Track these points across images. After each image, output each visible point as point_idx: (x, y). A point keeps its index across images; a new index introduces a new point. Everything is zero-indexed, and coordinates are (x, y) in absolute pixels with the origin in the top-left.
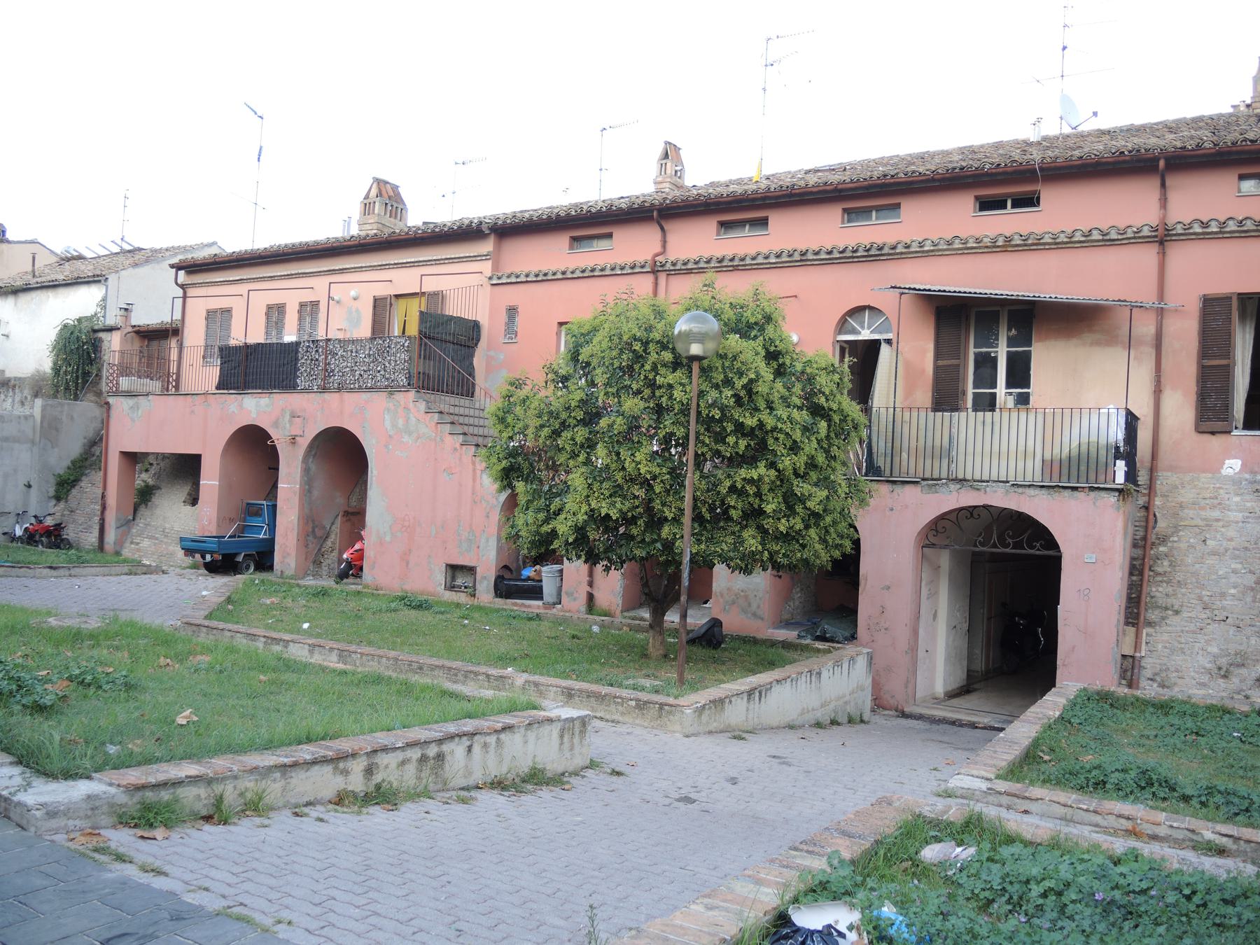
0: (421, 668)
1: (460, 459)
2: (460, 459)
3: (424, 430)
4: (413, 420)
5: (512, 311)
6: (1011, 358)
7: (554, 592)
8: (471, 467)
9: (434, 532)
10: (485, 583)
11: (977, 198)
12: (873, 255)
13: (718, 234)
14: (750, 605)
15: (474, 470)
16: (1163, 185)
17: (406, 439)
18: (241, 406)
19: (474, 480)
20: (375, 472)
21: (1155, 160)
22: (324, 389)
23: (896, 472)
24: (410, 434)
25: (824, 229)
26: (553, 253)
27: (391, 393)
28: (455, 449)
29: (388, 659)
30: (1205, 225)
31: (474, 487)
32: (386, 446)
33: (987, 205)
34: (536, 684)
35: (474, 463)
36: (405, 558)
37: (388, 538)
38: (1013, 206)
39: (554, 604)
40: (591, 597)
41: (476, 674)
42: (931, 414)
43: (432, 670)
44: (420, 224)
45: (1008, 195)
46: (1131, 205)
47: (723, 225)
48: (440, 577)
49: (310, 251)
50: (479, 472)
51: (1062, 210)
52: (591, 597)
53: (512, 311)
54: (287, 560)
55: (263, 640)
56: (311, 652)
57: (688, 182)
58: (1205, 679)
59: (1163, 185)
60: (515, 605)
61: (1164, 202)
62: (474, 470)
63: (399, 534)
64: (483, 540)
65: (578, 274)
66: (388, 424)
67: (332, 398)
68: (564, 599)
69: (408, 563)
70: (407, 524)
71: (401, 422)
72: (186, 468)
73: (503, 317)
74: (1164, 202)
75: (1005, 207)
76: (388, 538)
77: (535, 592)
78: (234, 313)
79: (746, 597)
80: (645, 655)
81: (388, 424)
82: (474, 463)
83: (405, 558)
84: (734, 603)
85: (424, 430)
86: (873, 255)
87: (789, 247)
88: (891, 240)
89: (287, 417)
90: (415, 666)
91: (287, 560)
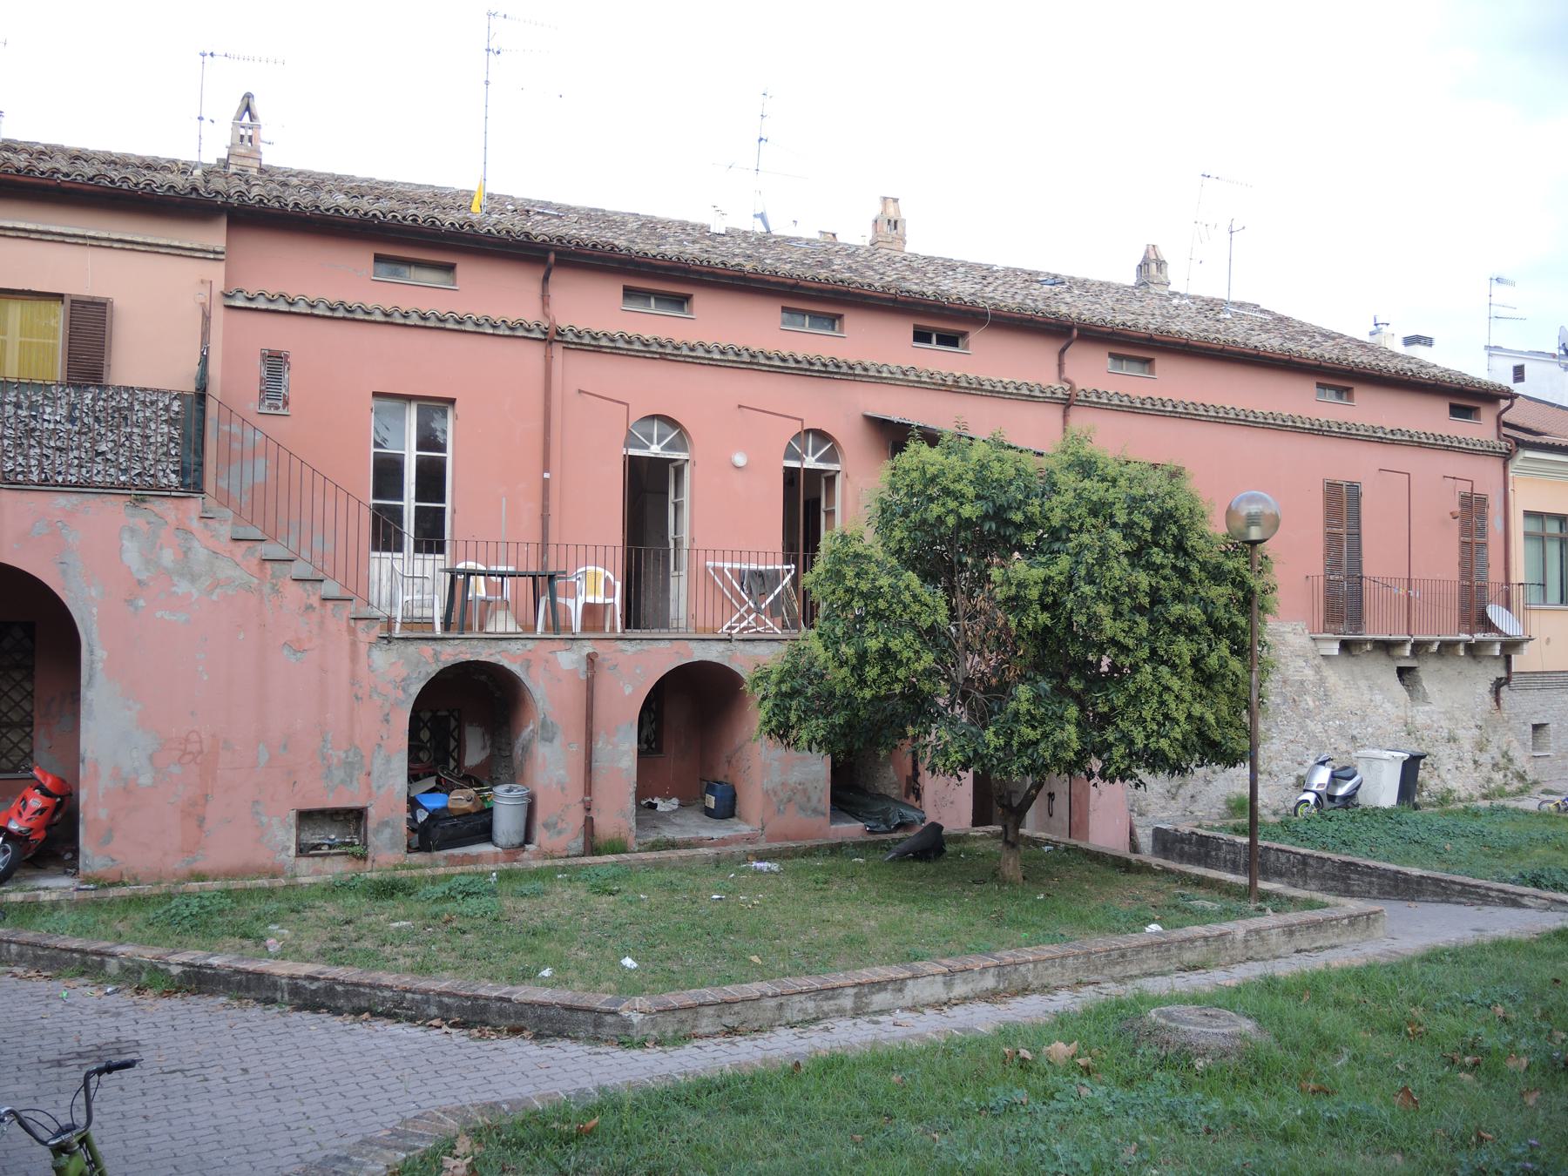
0: (1123, 956)
3: (226, 570)
5: (275, 362)
6: (422, 465)
7: (519, 824)
8: (346, 638)
9: (264, 758)
10: (387, 832)
11: (915, 326)
12: (831, 372)
13: (784, 323)
14: (809, 799)
15: (354, 644)
16: (546, 279)
17: (183, 587)
19: (354, 658)
20: (101, 654)
21: (1070, 328)
24: (193, 579)
25: (759, 327)
26: (347, 275)
27: (141, 499)
28: (310, 607)
29: (1076, 957)
30: (424, 317)
32: (130, 602)
33: (921, 336)
34: (1258, 932)
35: (352, 632)
36: (194, 814)
38: (939, 343)
39: (522, 845)
40: (589, 823)
41: (1192, 940)
43: (1138, 952)
45: (935, 330)
46: (1029, 363)
47: (629, 293)
48: (285, 836)
50: (363, 648)
51: (985, 357)
52: (589, 823)
53: (275, 362)
55: (852, 991)
56: (948, 985)
58: (1163, 802)
59: (546, 279)
60: (452, 861)
61: (545, 299)
62: (354, 644)
65: (414, 320)
68: (540, 834)
70: (194, 748)
71: (168, 557)
73: (257, 370)
74: (545, 299)
75: (930, 342)
76: (145, 780)
77: (480, 827)
79: (805, 791)
80: (995, 876)
83: (194, 814)
84: (790, 800)
86: (831, 372)
87: (739, 344)
88: (442, 310)
90: (1115, 954)
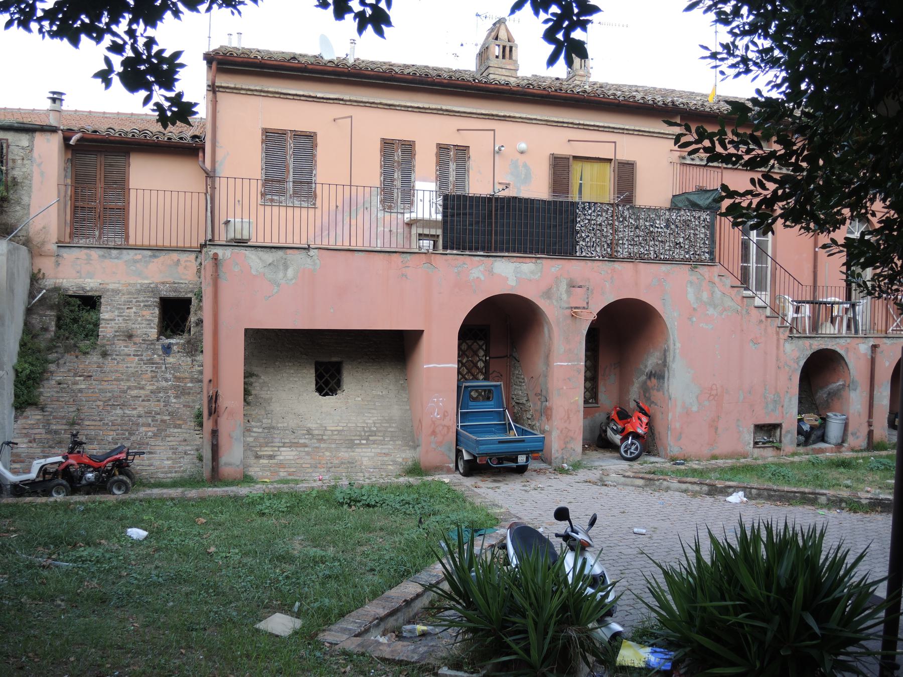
1: (766, 329)
2: (766, 329)
4: (718, 294)
8: (775, 336)
10: (789, 436)
15: (778, 340)
17: (711, 311)
18: (490, 271)
19: (778, 348)
22: (612, 258)
23: (216, 238)
28: (761, 321)
31: (777, 357)
32: (690, 319)
35: (778, 333)
36: (714, 426)
37: (695, 409)
42: (261, 209)
44: (529, 75)
48: (749, 437)
49: (433, 83)
50: (782, 341)
54: (572, 445)
57: (520, 74)
62: (778, 340)
63: (706, 403)
64: (787, 400)
66: (691, 296)
67: (625, 269)
69: (716, 429)
70: (714, 392)
71: (705, 296)
72: (392, 349)
76: (695, 409)
78: (418, 148)
81: (691, 296)
82: (778, 333)
83: (714, 426)
85: (729, 303)
89: (563, 287)
91: (572, 445)
